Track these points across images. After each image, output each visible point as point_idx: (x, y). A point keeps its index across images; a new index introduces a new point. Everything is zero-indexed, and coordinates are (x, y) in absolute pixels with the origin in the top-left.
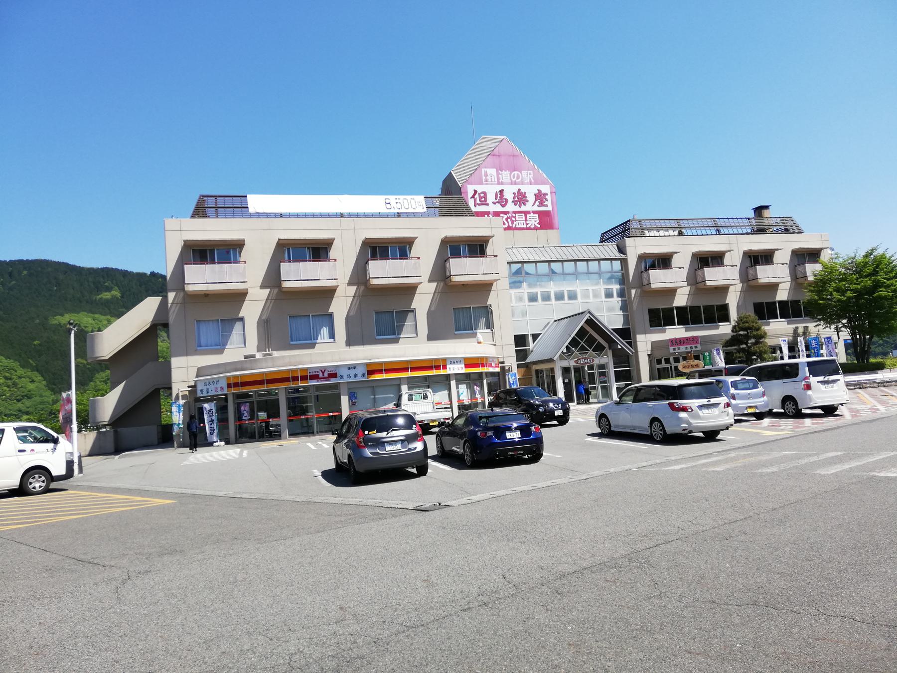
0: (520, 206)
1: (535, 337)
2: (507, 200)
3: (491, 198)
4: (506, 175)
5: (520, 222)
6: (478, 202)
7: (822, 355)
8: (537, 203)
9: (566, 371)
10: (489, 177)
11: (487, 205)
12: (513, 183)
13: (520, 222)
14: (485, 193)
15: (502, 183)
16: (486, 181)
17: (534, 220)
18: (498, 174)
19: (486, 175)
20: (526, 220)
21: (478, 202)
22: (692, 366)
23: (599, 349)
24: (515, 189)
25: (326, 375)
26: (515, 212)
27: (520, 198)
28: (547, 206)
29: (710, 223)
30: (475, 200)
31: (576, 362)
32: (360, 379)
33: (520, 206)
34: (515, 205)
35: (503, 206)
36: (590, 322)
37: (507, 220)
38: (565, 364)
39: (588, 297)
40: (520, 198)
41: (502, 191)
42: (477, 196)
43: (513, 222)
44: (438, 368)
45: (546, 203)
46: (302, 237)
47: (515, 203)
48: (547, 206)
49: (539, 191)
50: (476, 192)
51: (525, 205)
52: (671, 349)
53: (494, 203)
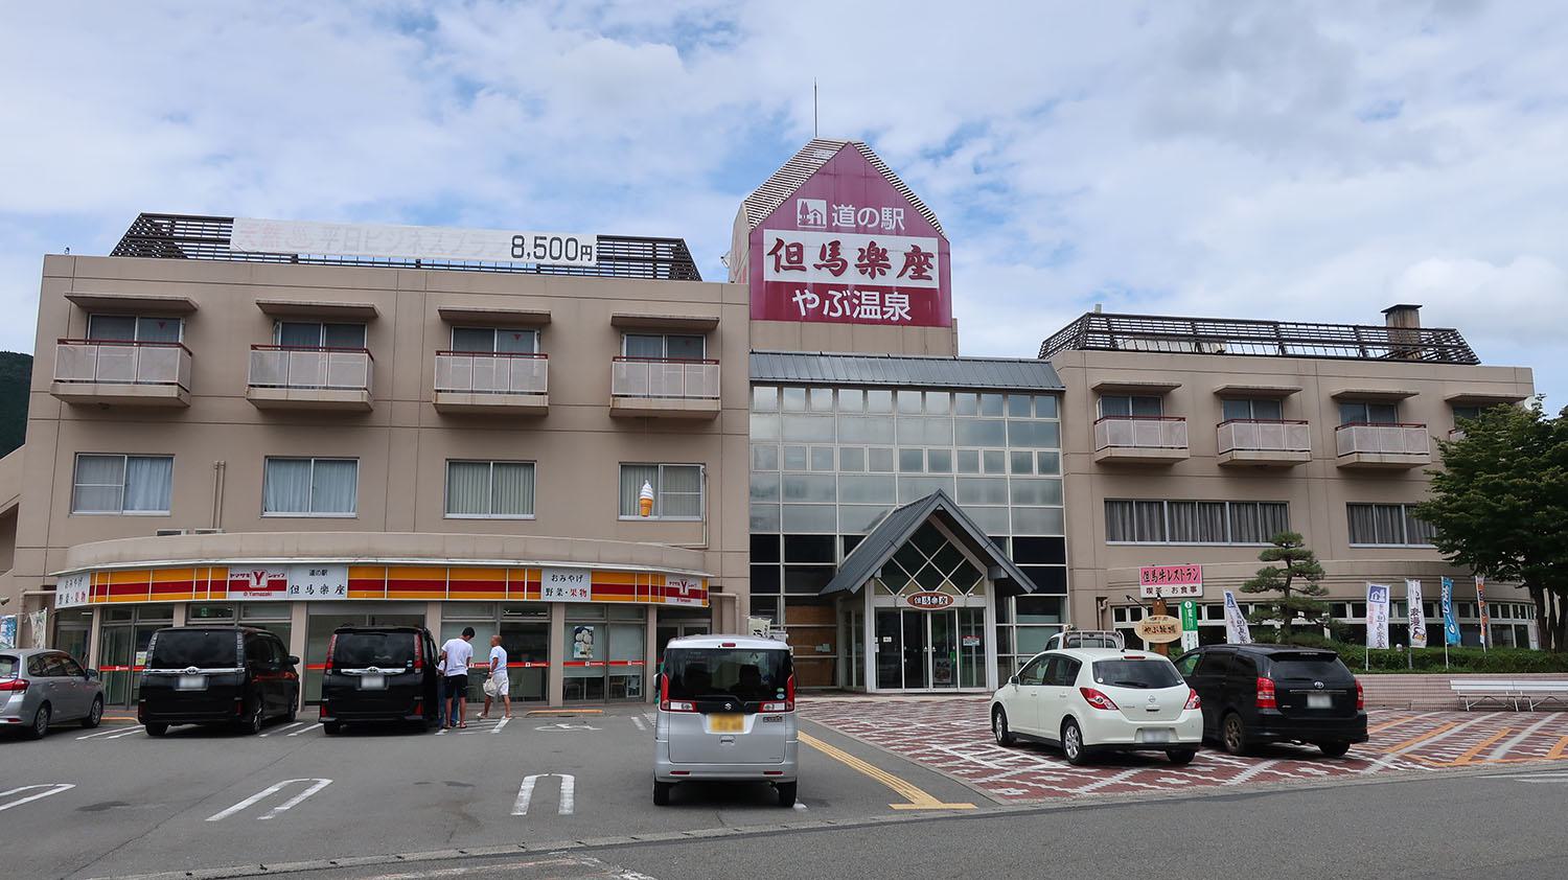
0: (873, 276)
1: (851, 542)
2: (845, 264)
3: (811, 257)
4: (846, 214)
5: (869, 309)
6: (784, 262)
7: (963, 636)
8: (910, 272)
9: (886, 620)
10: (811, 217)
11: (803, 269)
12: (858, 230)
13: (869, 309)
14: (800, 247)
15: (838, 230)
16: (805, 222)
17: (900, 307)
18: (830, 210)
19: (805, 210)
20: (882, 304)
21: (784, 262)
22: (1163, 630)
23: (965, 580)
24: (864, 241)
25: (264, 583)
26: (861, 288)
27: (874, 259)
28: (930, 278)
29: (1265, 331)
30: (778, 259)
31: (912, 600)
32: (332, 596)
33: (873, 276)
34: (863, 272)
35: (837, 274)
36: (942, 515)
37: (841, 301)
38: (887, 601)
39: (975, 468)
40: (874, 259)
41: (835, 245)
42: (782, 252)
43: (853, 307)
44: (516, 587)
45: (929, 273)
46: (480, 308)
47: (862, 269)
48: (930, 278)
49: (916, 249)
50: (780, 243)
51: (883, 273)
52: (1144, 588)
53: (818, 267)
